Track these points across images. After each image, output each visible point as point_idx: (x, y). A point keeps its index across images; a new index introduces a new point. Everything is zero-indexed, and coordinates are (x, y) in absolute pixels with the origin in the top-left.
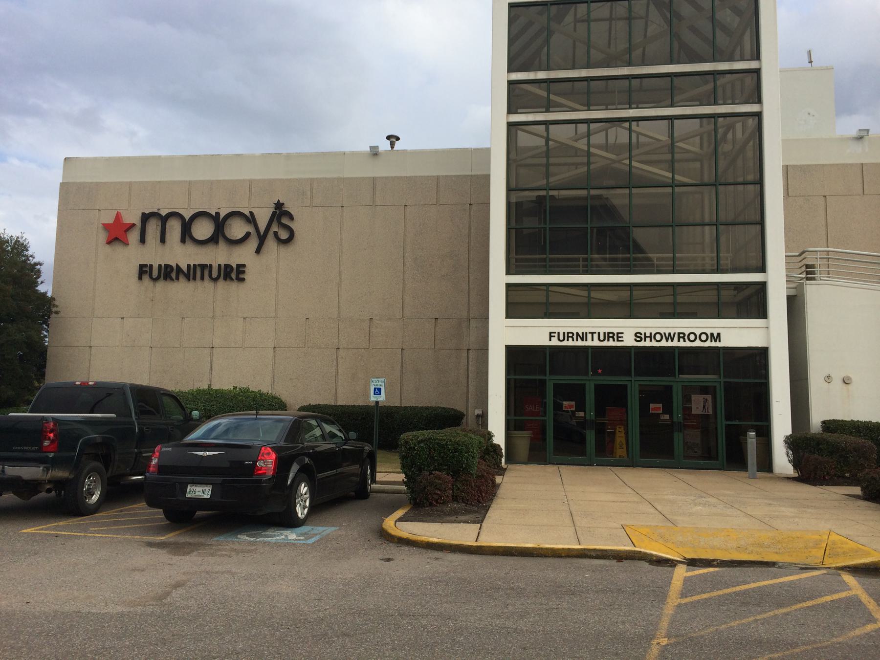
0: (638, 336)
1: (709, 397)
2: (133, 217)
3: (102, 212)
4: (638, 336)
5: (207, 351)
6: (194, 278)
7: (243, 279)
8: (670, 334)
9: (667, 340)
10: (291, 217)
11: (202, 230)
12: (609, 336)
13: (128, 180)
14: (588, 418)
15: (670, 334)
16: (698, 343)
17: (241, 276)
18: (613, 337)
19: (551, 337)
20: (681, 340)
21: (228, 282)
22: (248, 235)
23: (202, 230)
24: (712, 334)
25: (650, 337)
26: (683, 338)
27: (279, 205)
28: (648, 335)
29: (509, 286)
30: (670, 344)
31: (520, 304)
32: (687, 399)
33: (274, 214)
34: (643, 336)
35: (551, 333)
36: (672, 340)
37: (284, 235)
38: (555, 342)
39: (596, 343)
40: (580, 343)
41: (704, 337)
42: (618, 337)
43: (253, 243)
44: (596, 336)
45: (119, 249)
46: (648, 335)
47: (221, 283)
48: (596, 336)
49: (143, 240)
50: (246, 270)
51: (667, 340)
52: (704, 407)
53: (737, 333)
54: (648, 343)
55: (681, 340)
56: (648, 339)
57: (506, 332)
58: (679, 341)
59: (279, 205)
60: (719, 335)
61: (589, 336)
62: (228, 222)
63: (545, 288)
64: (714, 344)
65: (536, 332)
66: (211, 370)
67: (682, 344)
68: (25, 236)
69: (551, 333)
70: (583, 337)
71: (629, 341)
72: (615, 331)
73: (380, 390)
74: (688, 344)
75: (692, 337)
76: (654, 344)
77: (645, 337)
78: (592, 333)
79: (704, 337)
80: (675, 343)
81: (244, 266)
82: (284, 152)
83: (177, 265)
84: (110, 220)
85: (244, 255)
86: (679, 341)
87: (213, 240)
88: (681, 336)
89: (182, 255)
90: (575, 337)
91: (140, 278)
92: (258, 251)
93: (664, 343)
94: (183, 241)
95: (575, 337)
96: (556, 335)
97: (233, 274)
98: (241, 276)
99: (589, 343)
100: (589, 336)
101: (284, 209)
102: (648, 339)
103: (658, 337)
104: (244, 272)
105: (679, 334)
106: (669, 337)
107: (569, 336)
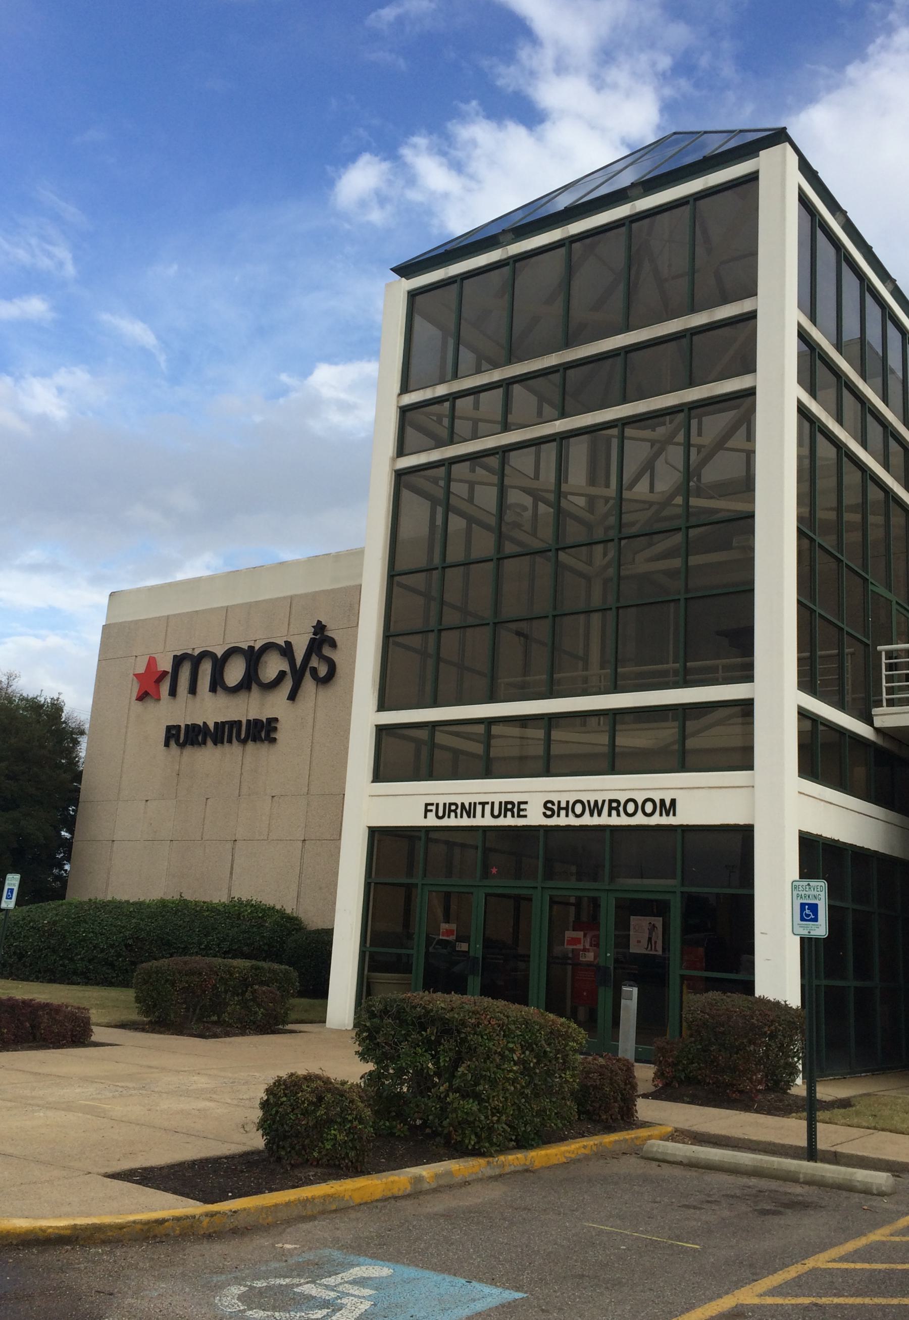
0: (550, 808)
1: (658, 922)
2: (165, 665)
3: (138, 659)
4: (550, 808)
5: (229, 846)
6: (222, 743)
7: (274, 740)
8: (596, 802)
9: (592, 815)
10: (333, 644)
11: (235, 673)
12: (508, 808)
13: (166, 614)
14: (472, 954)
15: (596, 802)
16: (640, 820)
17: (273, 735)
18: (512, 810)
19: (427, 811)
20: (614, 813)
21: (258, 745)
22: (282, 675)
23: (235, 673)
24: (662, 801)
25: (566, 809)
26: (617, 809)
27: (320, 628)
28: (563, 805)
29: (381, 730)
30: (596, 821)
31: (401, 754)
32: (623, 925)
33: (312, 641)
34: (555, 808)
35: (427, 805)
36: (599, 815)
37: (323, 671)
38: (432, 821)
39: (488, 821)
40: (465, 821)
41: (649, 807)
42: (519, 810)
43: (287, 685)
44: (488, 808)
45: (150, 705)
46: (563, 805)
47: (250, 745)
48: (488, 808)
49: (173, 693)
50: (278, 726)
51: (592, 815)
52: (650, 939)
53: (701, 799)
54: (562, 820)
55: (614, 813)
56: (563, 813)
57: (379, 803)
58: (610, 815)
59: (320, 628)
60: (673, 802)
61: (479, 808)
62: (264, 658)
63: (481, 729)
64: (665, 820)
65: (407, 805)
66: (231, 873)
67: (615, 820)
68: (62, 698)
69: (427, 805)
70: (469, 810)
71: (535, 817)
72: (516, 799)
73: (814, 908)
74: (624, 821)
75: (631, 808)
76: (572, 821)
77: (560, 808)
78: (483, 804)
79: (649, 807)
80: (604, 820)
81: (276, 720)
82: (333, 551)
83: (205, 723)
84: (141, 670)
85: (274, 705)
86: (610, 815)
87: (245, 685)
88: (614, 806)
89: (211, 709)
90: (459, 811)
91: (167, 744)
92: (292, 697)
93: (587, 820)
94: (213, 689)
95: (459, 811)
96: (434, 808)
97: (262, 732)
98: (273, 735)
99: (478, 821)
100: (479, 808)
101: (326, 633)
102: (563, 813)
103: (578, 809)
104: (275, 729)
105: (611, 801)
106: (595, 808)
107: (450, 809)
